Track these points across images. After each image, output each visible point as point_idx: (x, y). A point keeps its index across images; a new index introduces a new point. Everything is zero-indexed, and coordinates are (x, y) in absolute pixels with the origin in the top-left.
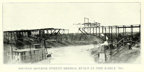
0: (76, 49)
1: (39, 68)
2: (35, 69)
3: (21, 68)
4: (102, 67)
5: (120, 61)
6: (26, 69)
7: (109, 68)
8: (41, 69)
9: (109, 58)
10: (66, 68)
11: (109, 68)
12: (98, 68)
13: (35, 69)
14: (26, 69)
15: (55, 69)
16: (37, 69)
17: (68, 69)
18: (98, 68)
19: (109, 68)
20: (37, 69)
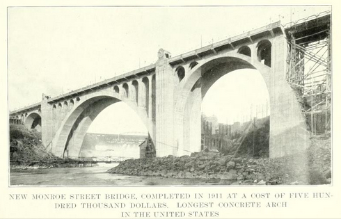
0: (274, 142)
1: (188, 204)
2: (36, 197)
3: (75, 196)
4: (63, 194)
5: (141, 152)
6: (226, 205)
7: (271, 205)
8: (50, 197)
9: (55, 141)
10: (110, 196)
11: (271, 205)
12: (85, 206)
13: (36, 197)
14: (226, 205)
15: (65, 206)
16: (41, 197)
17: (116, 197)
18: (85, 206)
19: (271, 205)
20: (41, 197)
